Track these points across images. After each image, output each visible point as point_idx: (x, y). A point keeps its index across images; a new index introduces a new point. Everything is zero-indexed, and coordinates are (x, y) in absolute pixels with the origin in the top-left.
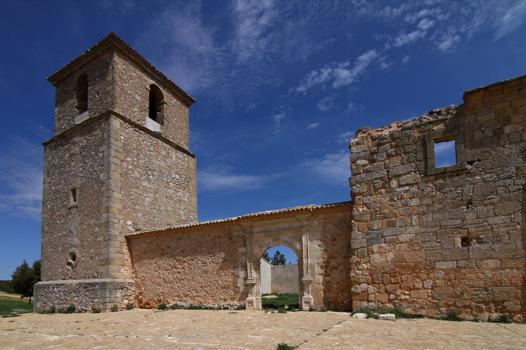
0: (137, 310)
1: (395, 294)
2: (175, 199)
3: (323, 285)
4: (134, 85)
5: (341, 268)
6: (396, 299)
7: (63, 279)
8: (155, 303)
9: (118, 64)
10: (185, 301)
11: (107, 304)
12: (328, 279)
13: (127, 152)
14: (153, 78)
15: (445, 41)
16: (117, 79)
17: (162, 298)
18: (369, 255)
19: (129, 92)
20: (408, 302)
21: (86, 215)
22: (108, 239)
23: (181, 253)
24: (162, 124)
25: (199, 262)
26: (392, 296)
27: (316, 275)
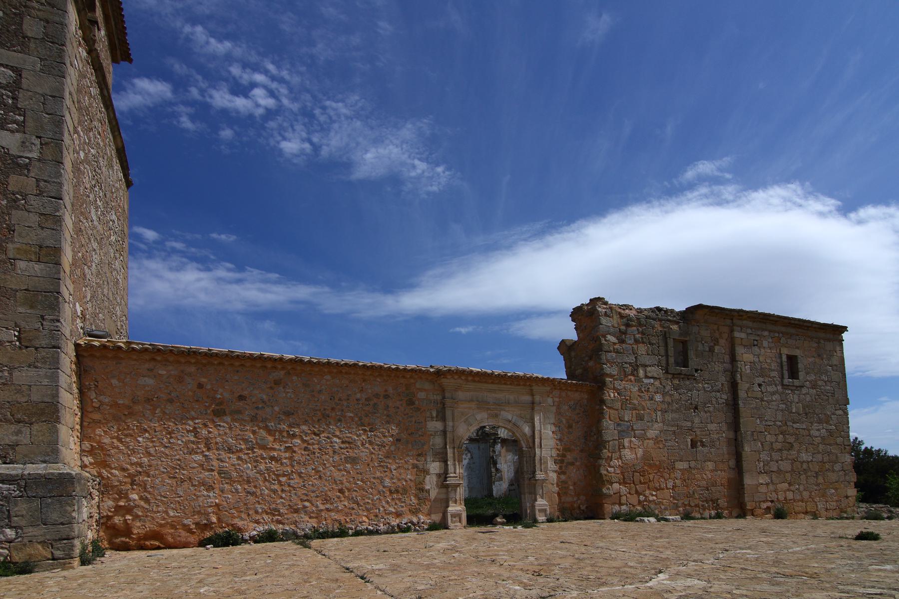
1: (644, 495)
3: (558, 486)
5: (578, 463)
6: (645, 500)
8: (183, 533)
12: (563, 477)
15: (289, 140)
17: (214, 519)
18: (619, 449)
20: (656, 504)
26: (642, 498)
27: (548, 473)
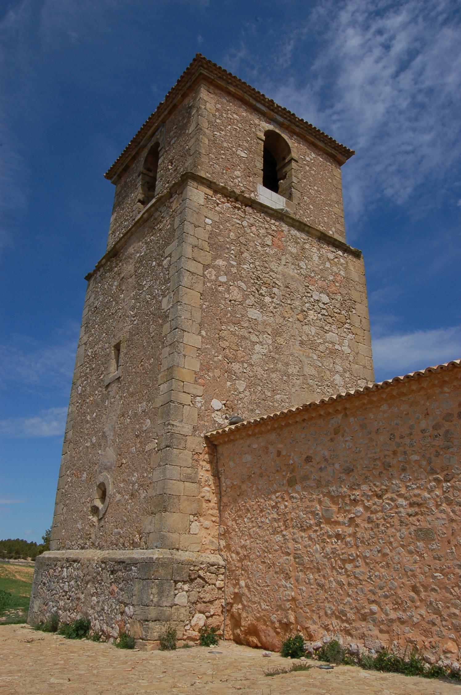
0: (228, 650)
2: (321, 348)
4: (234, 133)
7: (83, 548)
9: (206, 102)
10: (363, 637)
11: (151, 624)
13: (217, 248)
14: (270, 120)
16: (205, 124)
17: (292, 619)
19: (225, 144)
21: (132, 395)
22: (170, 442)
23: (344, 476)
24: (290, 197)
25: (401, 501)
